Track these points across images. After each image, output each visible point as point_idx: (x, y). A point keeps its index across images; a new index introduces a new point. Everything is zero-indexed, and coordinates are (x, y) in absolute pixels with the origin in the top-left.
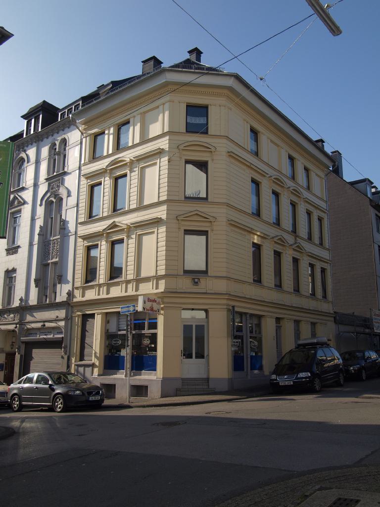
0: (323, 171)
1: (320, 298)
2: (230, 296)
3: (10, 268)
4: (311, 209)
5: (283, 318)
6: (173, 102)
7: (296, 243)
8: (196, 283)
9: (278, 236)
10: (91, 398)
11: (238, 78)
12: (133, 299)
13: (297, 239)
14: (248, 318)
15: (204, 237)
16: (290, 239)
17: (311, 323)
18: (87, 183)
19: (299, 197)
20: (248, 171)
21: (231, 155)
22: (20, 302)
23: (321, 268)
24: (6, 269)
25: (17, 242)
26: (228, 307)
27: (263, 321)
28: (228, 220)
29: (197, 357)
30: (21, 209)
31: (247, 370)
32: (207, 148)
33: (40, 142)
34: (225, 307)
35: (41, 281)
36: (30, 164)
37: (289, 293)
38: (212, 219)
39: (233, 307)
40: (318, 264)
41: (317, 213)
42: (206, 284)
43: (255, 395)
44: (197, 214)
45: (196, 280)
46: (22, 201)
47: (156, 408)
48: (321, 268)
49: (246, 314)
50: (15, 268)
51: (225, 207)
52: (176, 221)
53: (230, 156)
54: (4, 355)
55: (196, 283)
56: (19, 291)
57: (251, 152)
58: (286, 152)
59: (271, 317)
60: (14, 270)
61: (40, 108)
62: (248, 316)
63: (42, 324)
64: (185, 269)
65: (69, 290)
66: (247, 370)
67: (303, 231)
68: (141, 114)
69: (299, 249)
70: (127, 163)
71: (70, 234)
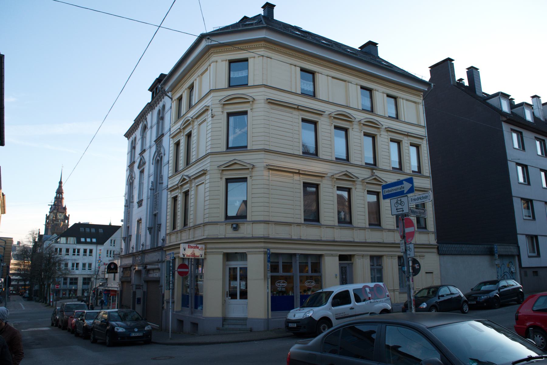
0: (419, 96)
5: (354, 255)
6: (217, 62)
7: (373, 175)
8: (236, 229)
9: (343, 172)
11: (202, 37)
18: (173, 142)
19: (378, 128)
20: (296, 113)
21: (271, 102)
25: (296, 176)
26: (266, 250)
29: (241, 298)
32: (245, 100)
33: (154, 110)
35: (153, 228)
36: (148, 130)
38: (249, 166)
42: (246, 230)
49: (295, 255)
53: (269, 102)
55: (236, 229)
56: (142, 240)
57: (304, 94)
58: (357, 85)
59: (332, 255)
68: (199, 76)
70: (190, 122)
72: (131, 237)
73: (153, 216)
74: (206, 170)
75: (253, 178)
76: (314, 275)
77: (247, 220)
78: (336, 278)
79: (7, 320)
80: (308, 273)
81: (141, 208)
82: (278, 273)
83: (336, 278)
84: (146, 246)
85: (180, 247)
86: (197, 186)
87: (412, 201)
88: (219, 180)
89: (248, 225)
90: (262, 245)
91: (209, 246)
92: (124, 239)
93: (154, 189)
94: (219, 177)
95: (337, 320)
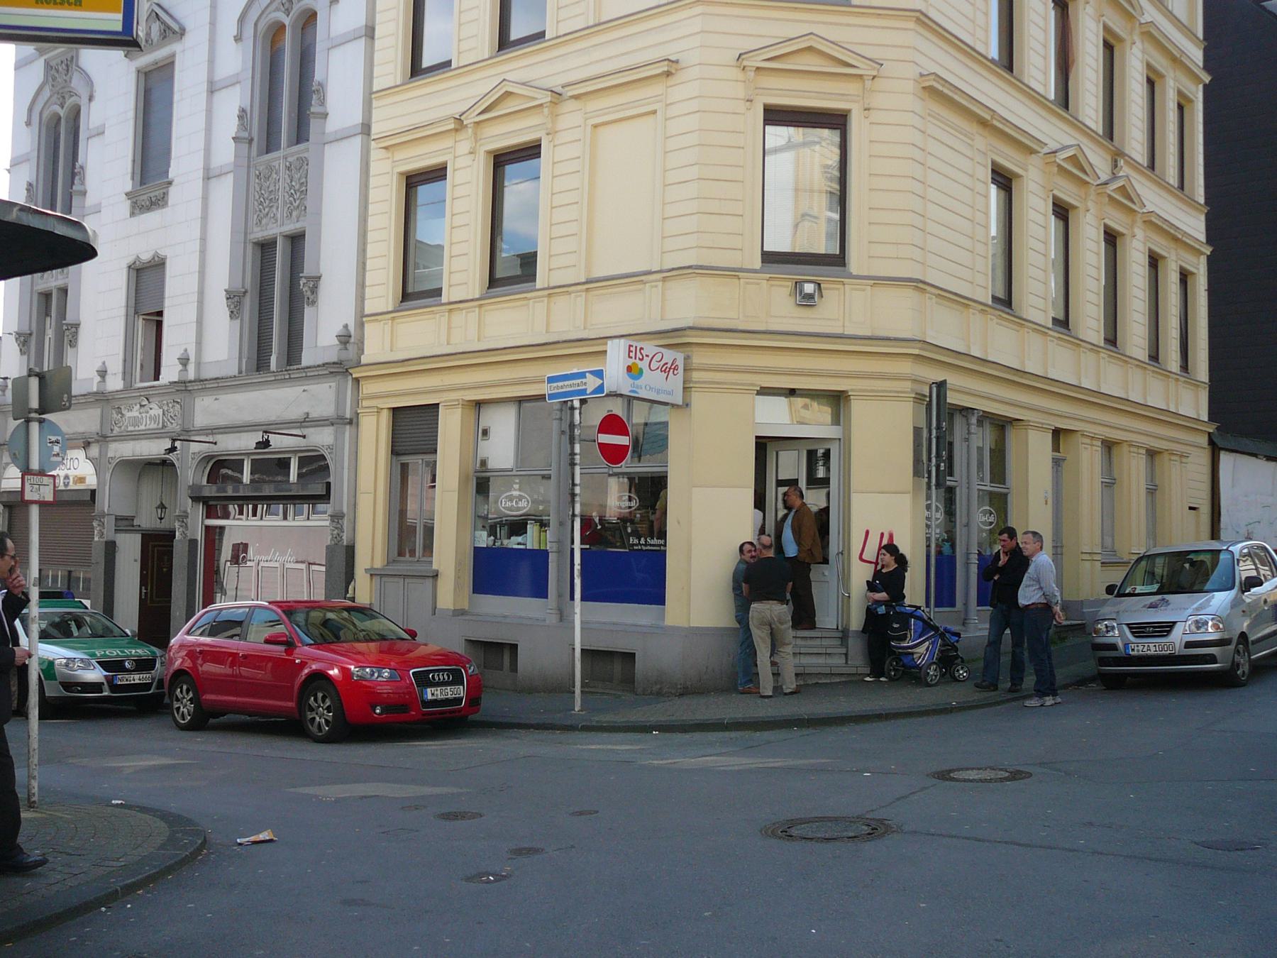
1: (1174, 370)
2: (927, 353)
3: (146, 257)
4: (1161, 63)
9: (1065, 148)
10: (430, 693)
12: (593, 347)
13: (1121, 162)
14: (973, 428)
15: (828, 137)
16: (1098, 160)
17: (1148, 450)
22: (180, 367)
23: (1182, 268)
24: (130, 260)
27: (1012, 436)
28: (922, 75)
30: (173, 55)
31: (966, 604)
34: (908, 385)
37: (1094, 347)
39: (941, 385)
40: (1174, 258)
41: (1175, 80)
43: (5, 495)
44: (810, 49)
45: (809, 288)
46: (175, 27)
47: (687, 736)
48: (1182, 268)
50: (162, 253)
51: (911, 25)
52: (736, 73)
54: (138, 537)
55: (807, 301)
59: (1040, 428)
60: (158, 265)
61: (212, 721)
62: (974, 420)
63: (258, 437)
64: (765, 249)
65: (346, 326)
66: (966, 604)
67: (1135, 142)
69: (1126, 200)
71: (301, 275)
72: (76, 333)
73: (250, 248)
74: (677, 62)
75: (875, 117)
76: (417, 541)
77: (844, 271)
78: (1046, 504)
79: (761, 547)
80: (1004, 484)
81: (152, 219)
82: (418, 529)
83: (1046, 504)
84: (198, 364)
85: (606, 351)
86: (595, 126)
87: (632, 354)
88: (741, 106)
89: (856, 289)
90: (906, 367)
91: (699, 358)
92: (22, 339)
93: (251, 141)
94: (742, 94)
95: (1239, 632)
